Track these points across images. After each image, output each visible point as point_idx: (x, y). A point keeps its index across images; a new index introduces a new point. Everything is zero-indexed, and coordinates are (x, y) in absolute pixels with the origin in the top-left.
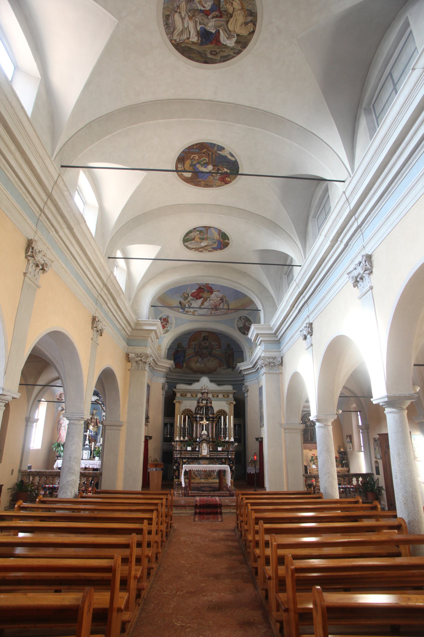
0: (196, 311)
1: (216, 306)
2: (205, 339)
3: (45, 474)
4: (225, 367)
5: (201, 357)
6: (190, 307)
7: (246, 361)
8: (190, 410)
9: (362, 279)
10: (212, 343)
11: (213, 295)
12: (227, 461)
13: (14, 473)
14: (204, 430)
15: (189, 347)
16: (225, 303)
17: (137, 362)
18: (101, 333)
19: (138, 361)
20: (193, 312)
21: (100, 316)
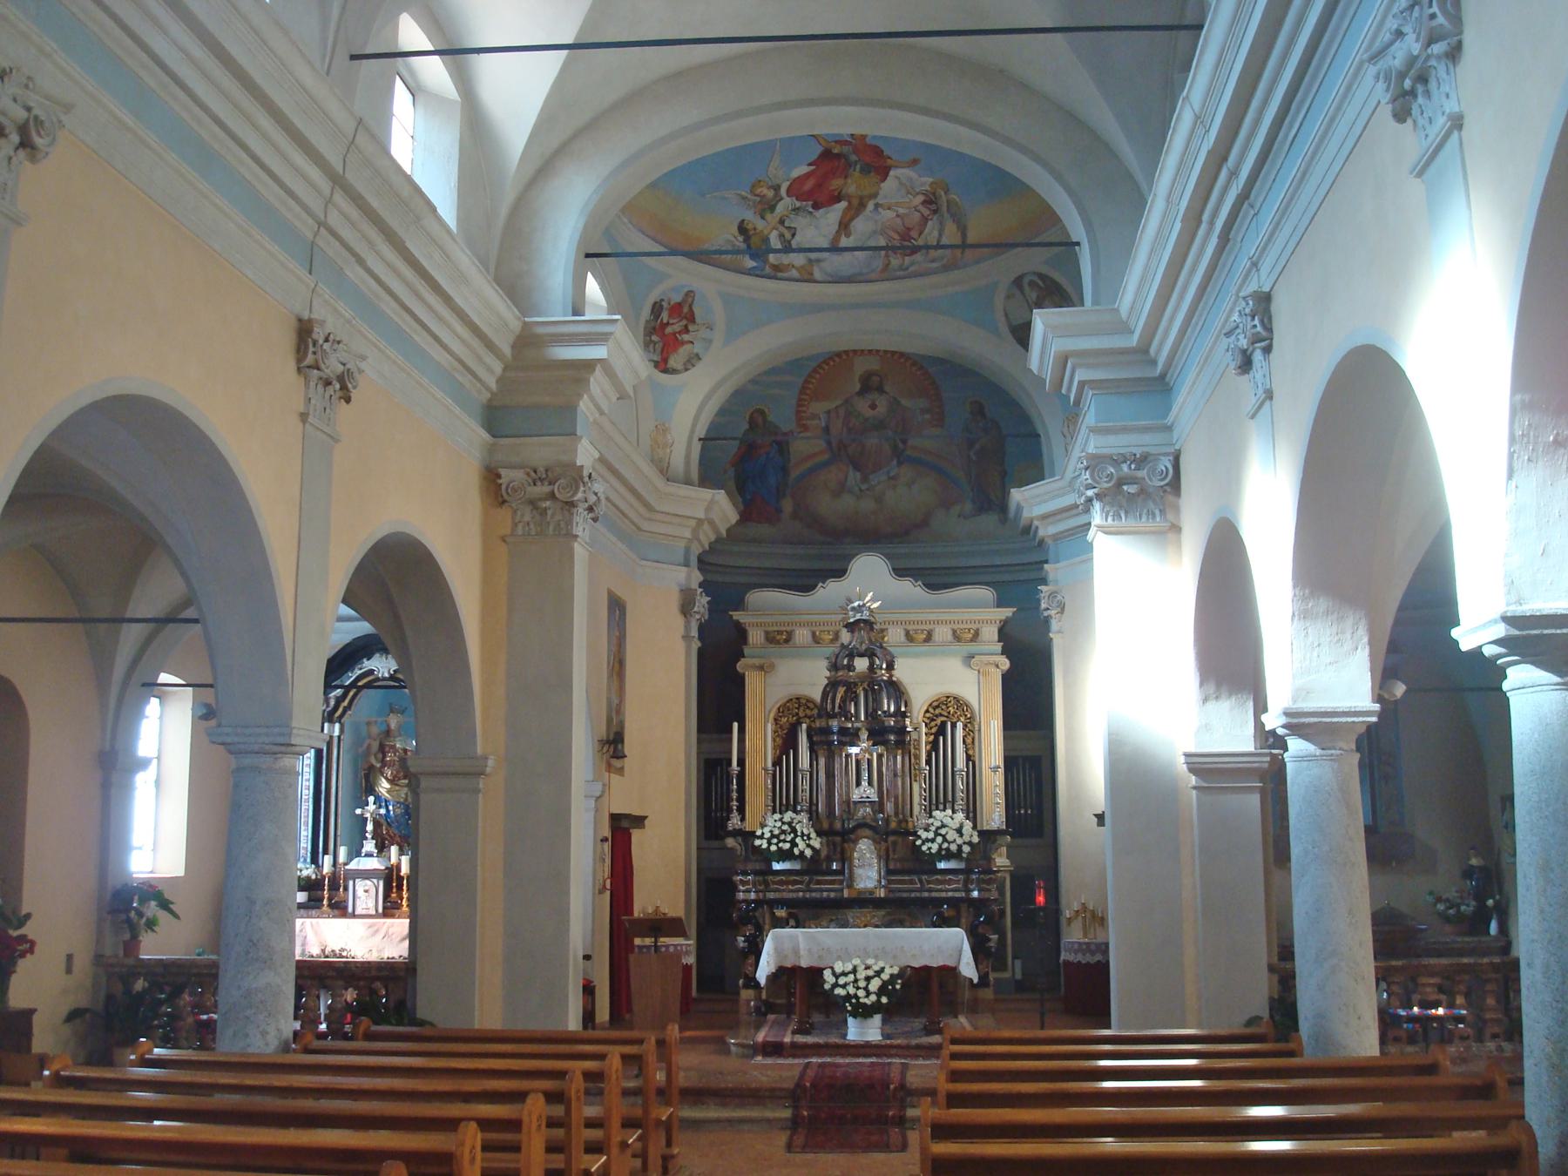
0: (818, 261)
1: (905, 235)
2: (869, 385)
3: (195, 971)
5: (857, 467)
6: (787, 249)
7: (1052, 475)
8: (808, 701)
9: (1423, 79)
10: (905, 402)
11: (889, 185)
13: (78, 964)
14: (865, 783)
15: (806, 428)
17: (533, 503)
18: (344, 387)
19: (540, 499)
20: (802, 267)
21: (331, 316)
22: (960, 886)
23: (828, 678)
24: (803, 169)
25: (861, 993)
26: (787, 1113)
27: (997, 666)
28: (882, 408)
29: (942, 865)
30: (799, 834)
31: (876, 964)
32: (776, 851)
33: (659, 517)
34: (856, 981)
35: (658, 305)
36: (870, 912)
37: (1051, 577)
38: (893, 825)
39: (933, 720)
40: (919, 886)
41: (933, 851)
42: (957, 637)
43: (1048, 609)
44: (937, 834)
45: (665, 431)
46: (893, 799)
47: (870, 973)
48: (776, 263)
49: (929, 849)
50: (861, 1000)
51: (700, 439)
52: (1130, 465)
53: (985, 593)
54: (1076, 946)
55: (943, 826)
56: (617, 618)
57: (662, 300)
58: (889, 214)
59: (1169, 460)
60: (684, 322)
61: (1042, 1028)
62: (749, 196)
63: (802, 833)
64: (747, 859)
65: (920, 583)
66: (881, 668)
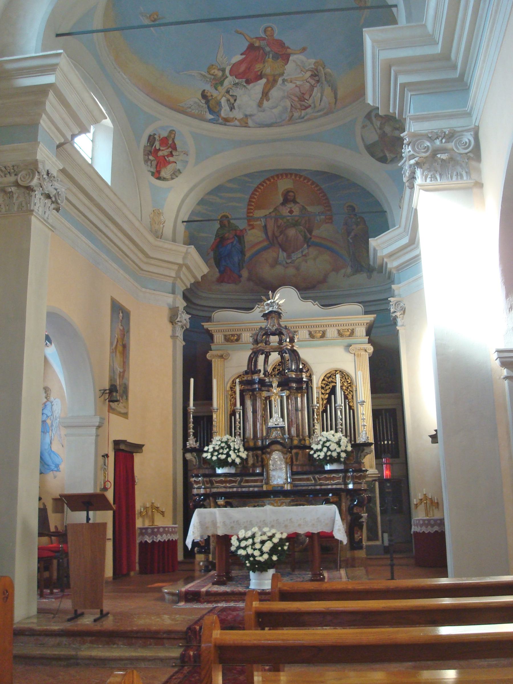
1: (302, 99)
4: (349, 270)
5: (284, 250)
10: (309, 209)
11: (290, 67)
12: (344, 500)
15: (252, 227)
16: (325, 83)
20: (242, 119)
22: (341, 481)
23: (252, 349)
24: (238, 58)
26: (176, 653)
27: (366, 351)
29: (328, 467)
30: (232, 449)
31: (270, 531)
32: (216, 460)
33: (153, 262)
34: (254, 544)
35: (152, 137)
36: (279, 500)
37: (396, 292)
38: (296, 442)
39: (327, 385)
40: (313, 482)
41: (321, 457)
42: (340, 334)
43: (395, 312)
44: (323, 446)
45: (160, 214)
47: (265, 538)
48: (225, 117)
49: (319, 456)
50: (257, 559)
51: (183, 222)
52: (442, 140)
53: (358, 308)
54: (421, 522)
55: (328, 441)
56: (121, 318)
57: (155, 134)
58: (292, 86)
59: (471, 134)
60: (170, 150)
61: (392, 578)
62: (207, 75)
64: (200, 468)
66: (286, 341)
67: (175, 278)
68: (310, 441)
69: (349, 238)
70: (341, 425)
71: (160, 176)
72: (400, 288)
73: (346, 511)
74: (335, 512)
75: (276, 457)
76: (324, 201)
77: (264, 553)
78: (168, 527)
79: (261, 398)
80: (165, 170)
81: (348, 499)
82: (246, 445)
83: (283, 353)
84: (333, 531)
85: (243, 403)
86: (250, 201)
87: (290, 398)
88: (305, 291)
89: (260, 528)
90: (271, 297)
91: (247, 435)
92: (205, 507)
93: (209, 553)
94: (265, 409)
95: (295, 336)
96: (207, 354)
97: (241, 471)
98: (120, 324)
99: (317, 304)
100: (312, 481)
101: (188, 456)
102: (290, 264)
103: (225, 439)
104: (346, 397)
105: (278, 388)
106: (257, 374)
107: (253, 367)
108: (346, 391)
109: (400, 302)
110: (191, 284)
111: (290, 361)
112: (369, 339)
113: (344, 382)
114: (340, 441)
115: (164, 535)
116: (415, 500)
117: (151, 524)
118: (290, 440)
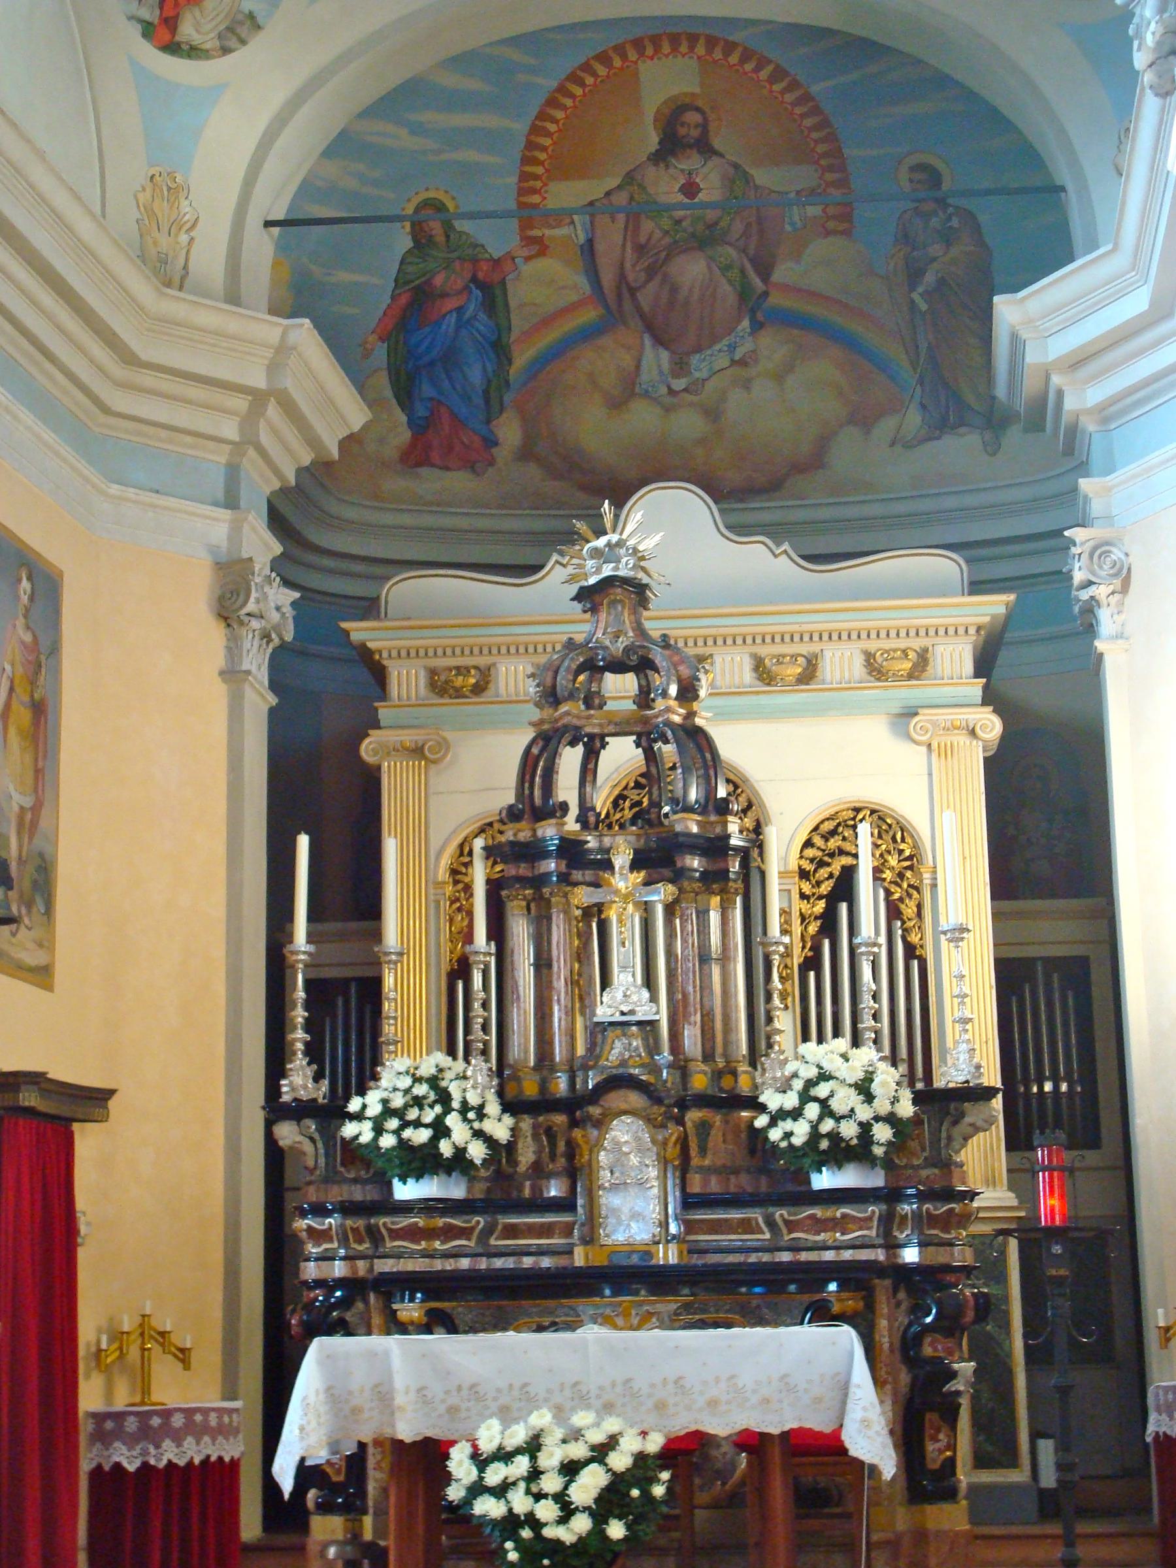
4: (914, 419)
7: (1093, 245)
10: (762, 176)
12: (883, 1307)
15: (540, 248)
22: (874, 1233)
25: (547, 1511)
27: (973, 733)
28: (711, 186)
29: (824, 1180)
30: (456, 1104)
32: (393, 1148)
33: (148, 379)
34: (535, 1474)
38: (699, 1082)
39: (821, 864)
40: (767, 1236)
41: (797, 1141)
42: (875, 669)
43: (1090, 583)
44: (806, 1097)
45: (175, 191)
46: (698, 1017)
47: (578, 1451)
49: (788, 1135)
50: (548, 1532)
51: (268, 224)
55: (824, 1077)
56: (25, 599)
63: (464, 1103)
64: (332, 1177)
65: (786, 546)
66: (665, 694)
67: (238, 448)
68: (753, 1079)
69: (915, 296)
70: (876, 1017)
71: (177, 38)
72: (1110, 489)
73: (892, 1350)
74: (851, 1355)
75: (626, 1138)
76: (821, 148)
77: (577, 1508)
78: (205, 1412)
79: (566, 912)
80: (197, 13)
81: (898, 1304)
82: (510, 1093)
83: (655, 741)
84: (841, 1426)
85: (498, 931)
86: (530, 145)
87: (678, 913)
88: (742, 501)
89: (560, 1414)
90: (608, 525)
91: (514, 1053)
92: (347, 1330)
93: (365, 1512)
94: (581, 956)
95: (702, 676)
96: (360, 744)
97: (489, 1191)
98: (20, 622)
99: (785, 552)
100: (763, 1233)
101: (287, 1133)
102: (686, 395)
103: (427, 1068)
104: (894, 912)
105: (635, 874)
106: (553, 821)
107: (537, 793)
108: (893, 888)
109: (1108, 543)
110: (300, 471)
111: (679, 771)
112: (986, 688)
113: (889, 852)
114: (869, 1078)
115: (189, 1441)
116: (1160, 1311)
117: (138, 1399)
118: (678, 1073)
